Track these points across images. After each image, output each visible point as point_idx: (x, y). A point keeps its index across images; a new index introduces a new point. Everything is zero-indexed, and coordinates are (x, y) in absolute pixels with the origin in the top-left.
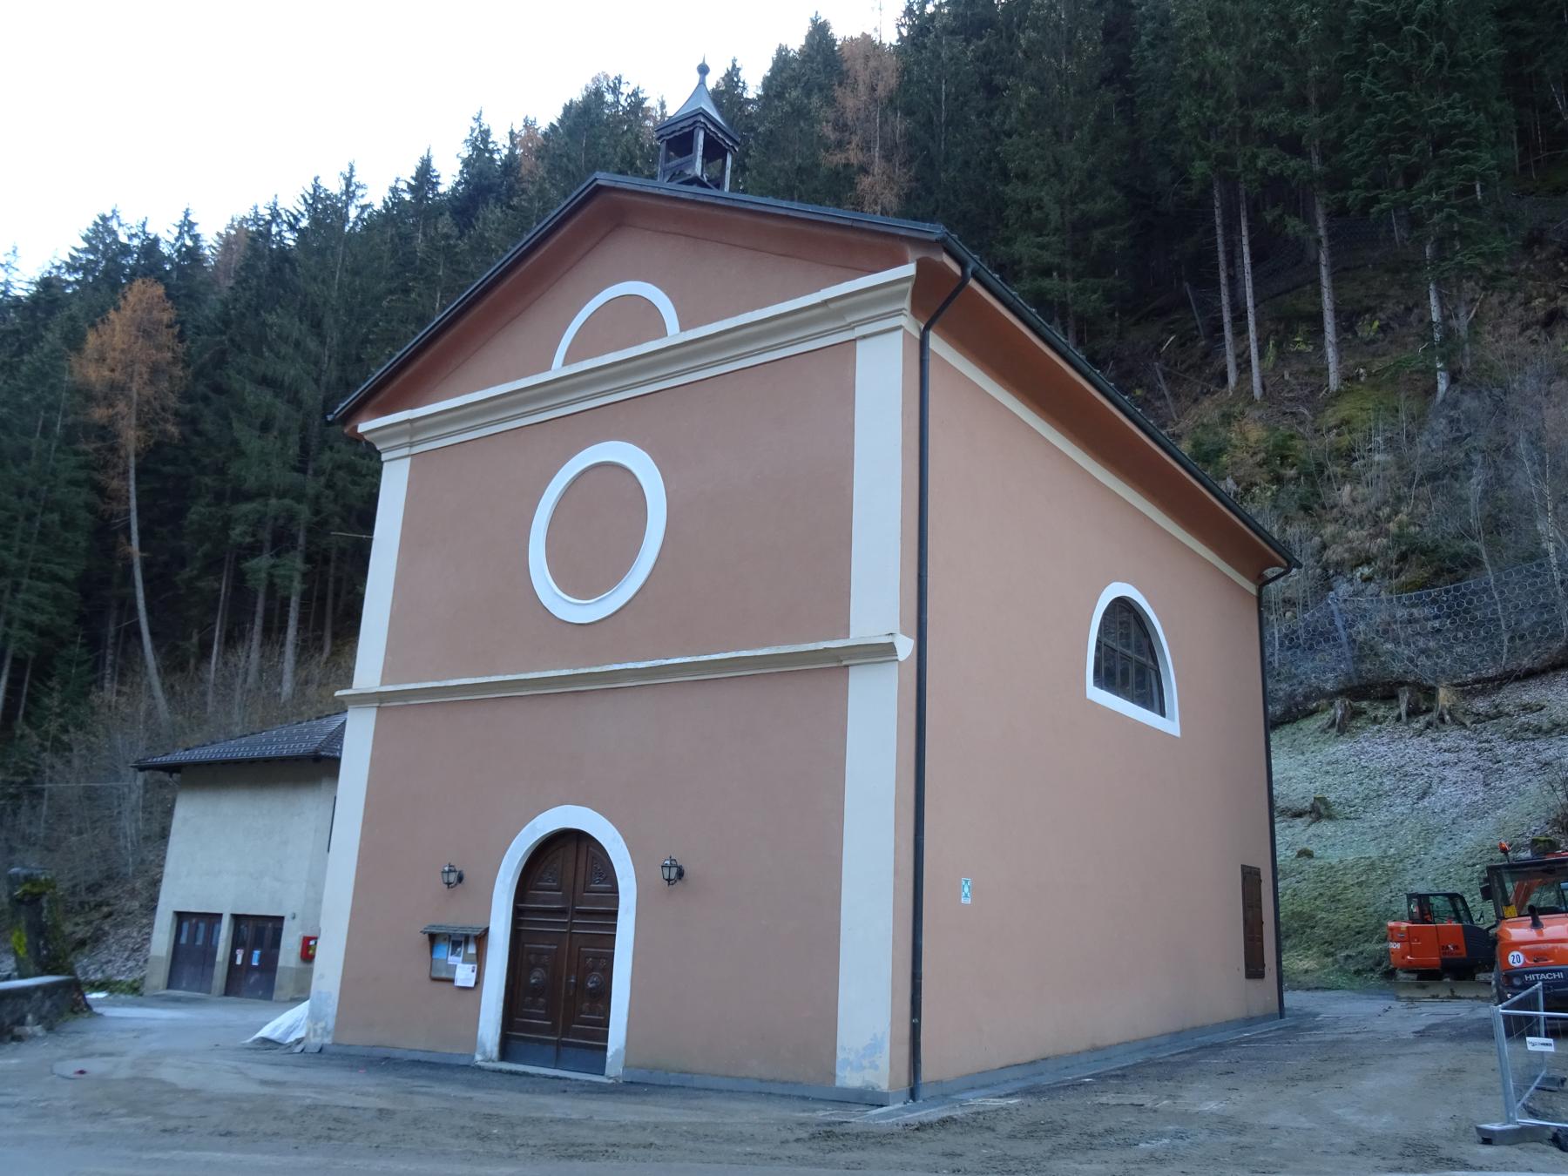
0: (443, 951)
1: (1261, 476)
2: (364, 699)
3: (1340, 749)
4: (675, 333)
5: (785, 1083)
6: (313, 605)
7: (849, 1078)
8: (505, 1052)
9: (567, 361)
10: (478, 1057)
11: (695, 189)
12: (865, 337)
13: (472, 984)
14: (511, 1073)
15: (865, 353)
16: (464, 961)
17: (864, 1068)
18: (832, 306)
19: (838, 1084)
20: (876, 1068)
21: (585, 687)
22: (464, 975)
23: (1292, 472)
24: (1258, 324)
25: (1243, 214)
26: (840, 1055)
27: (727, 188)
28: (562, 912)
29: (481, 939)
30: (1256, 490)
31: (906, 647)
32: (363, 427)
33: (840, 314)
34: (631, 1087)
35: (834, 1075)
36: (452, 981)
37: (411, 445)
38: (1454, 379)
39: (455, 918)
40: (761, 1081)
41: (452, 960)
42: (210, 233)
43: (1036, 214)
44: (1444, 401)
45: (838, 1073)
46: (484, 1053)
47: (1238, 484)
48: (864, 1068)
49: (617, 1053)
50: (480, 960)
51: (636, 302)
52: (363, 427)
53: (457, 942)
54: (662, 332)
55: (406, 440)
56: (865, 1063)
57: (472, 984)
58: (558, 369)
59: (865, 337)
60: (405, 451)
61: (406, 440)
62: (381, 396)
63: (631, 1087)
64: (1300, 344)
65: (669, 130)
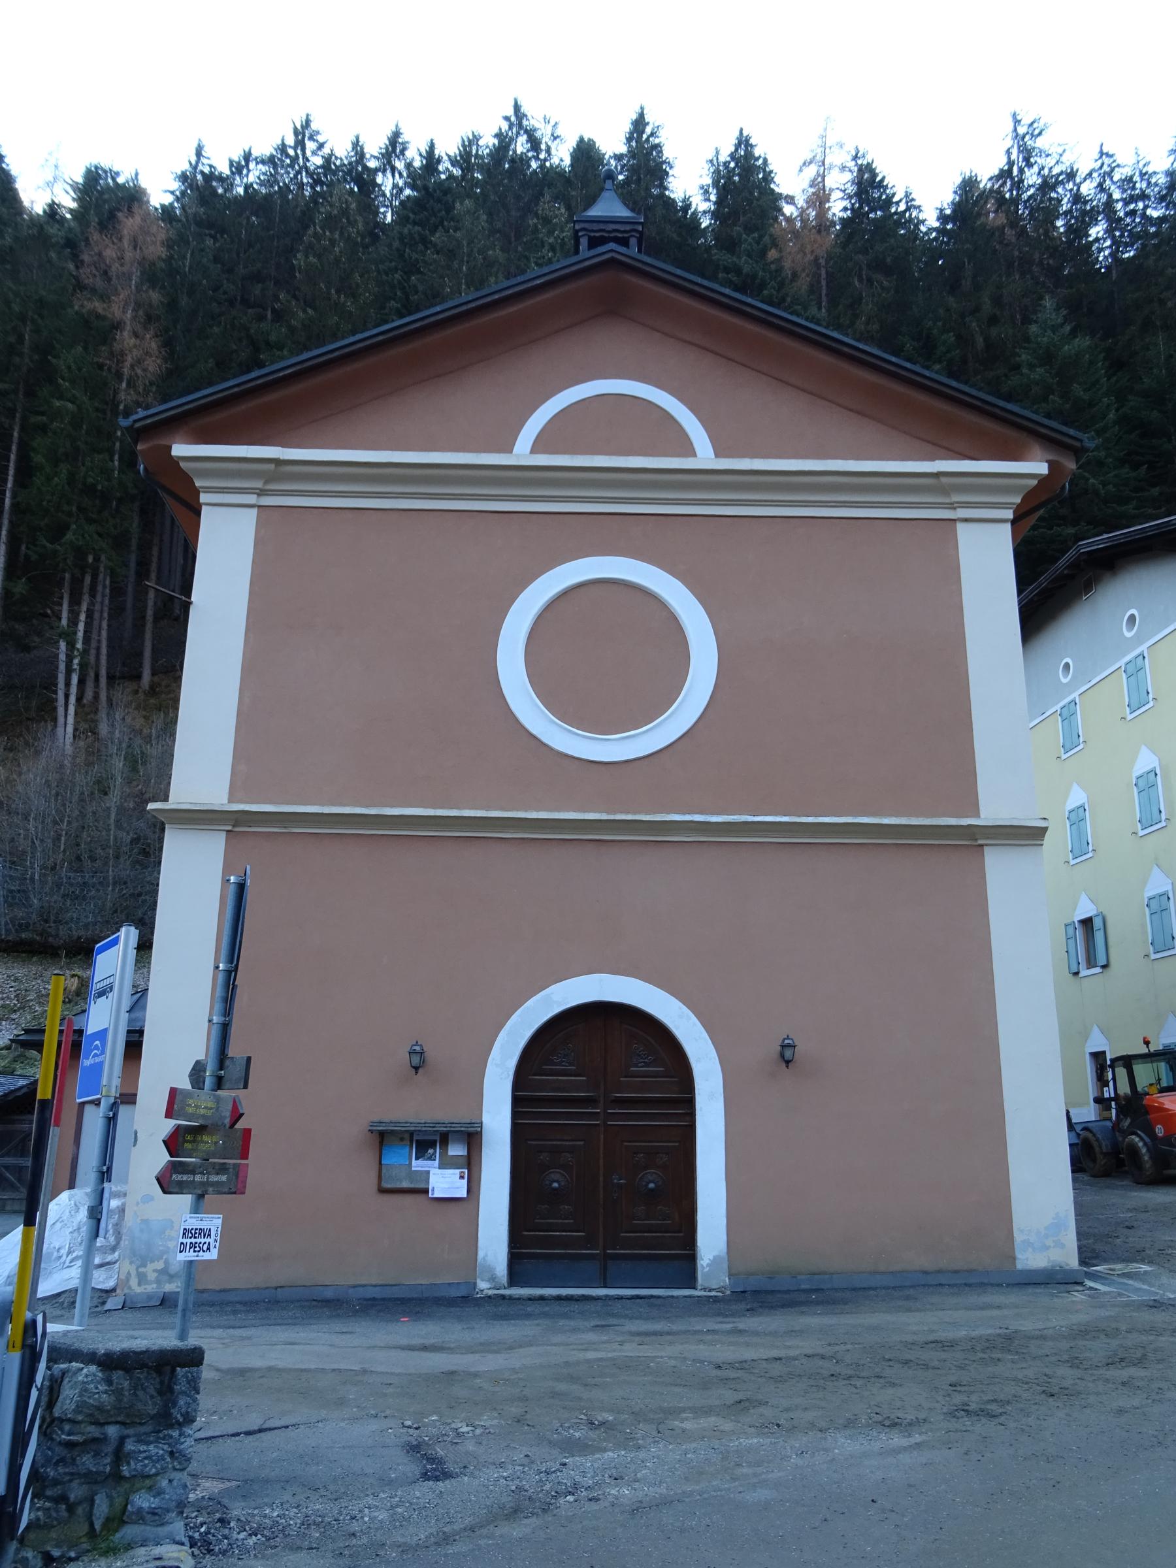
2: (199, 818)
3: (6, 1274)
4: (705, 455)
5: (956, 1272)
6: (124, 670)
7: (1030, 1259)
8: (516, 1275)
9: (539, 446)
10: (483, 1285)
12: (966, 520)
13: (463, 1193)
14: (559, 1298)
15: (965, 534)
17: (1048, 1248)
18: (944, 480)
19: (1019, 1266)
20: (1062, 1246)
21: (610, 837)
22: (445, 1182)
26: (1018, 1237)
29: (473, 1138)
32: (179, 450)
33: (945, 491)
34: (715, 1305)
35: (1014, 1259)
36: (426, 1191)
37: (261, 493)
39: (417, 1108)
40: (925, 1273)
42: (928, 195)
45: (1019, 1255)
46: (492, 1279)
48: (1048, 1248)
49: (716, 1261)
50: (471, 1165)
52: (179, 450)
53: (427, 1141)
55: (259, 484)
56: (1049, 1242)
57: (463, 1193)
58: (522, 451)
59: (966, 520)
60: (252, 499)
61: (259, 484)
62: (218, 417)
63: (715, 1305)
65: (595, 227)
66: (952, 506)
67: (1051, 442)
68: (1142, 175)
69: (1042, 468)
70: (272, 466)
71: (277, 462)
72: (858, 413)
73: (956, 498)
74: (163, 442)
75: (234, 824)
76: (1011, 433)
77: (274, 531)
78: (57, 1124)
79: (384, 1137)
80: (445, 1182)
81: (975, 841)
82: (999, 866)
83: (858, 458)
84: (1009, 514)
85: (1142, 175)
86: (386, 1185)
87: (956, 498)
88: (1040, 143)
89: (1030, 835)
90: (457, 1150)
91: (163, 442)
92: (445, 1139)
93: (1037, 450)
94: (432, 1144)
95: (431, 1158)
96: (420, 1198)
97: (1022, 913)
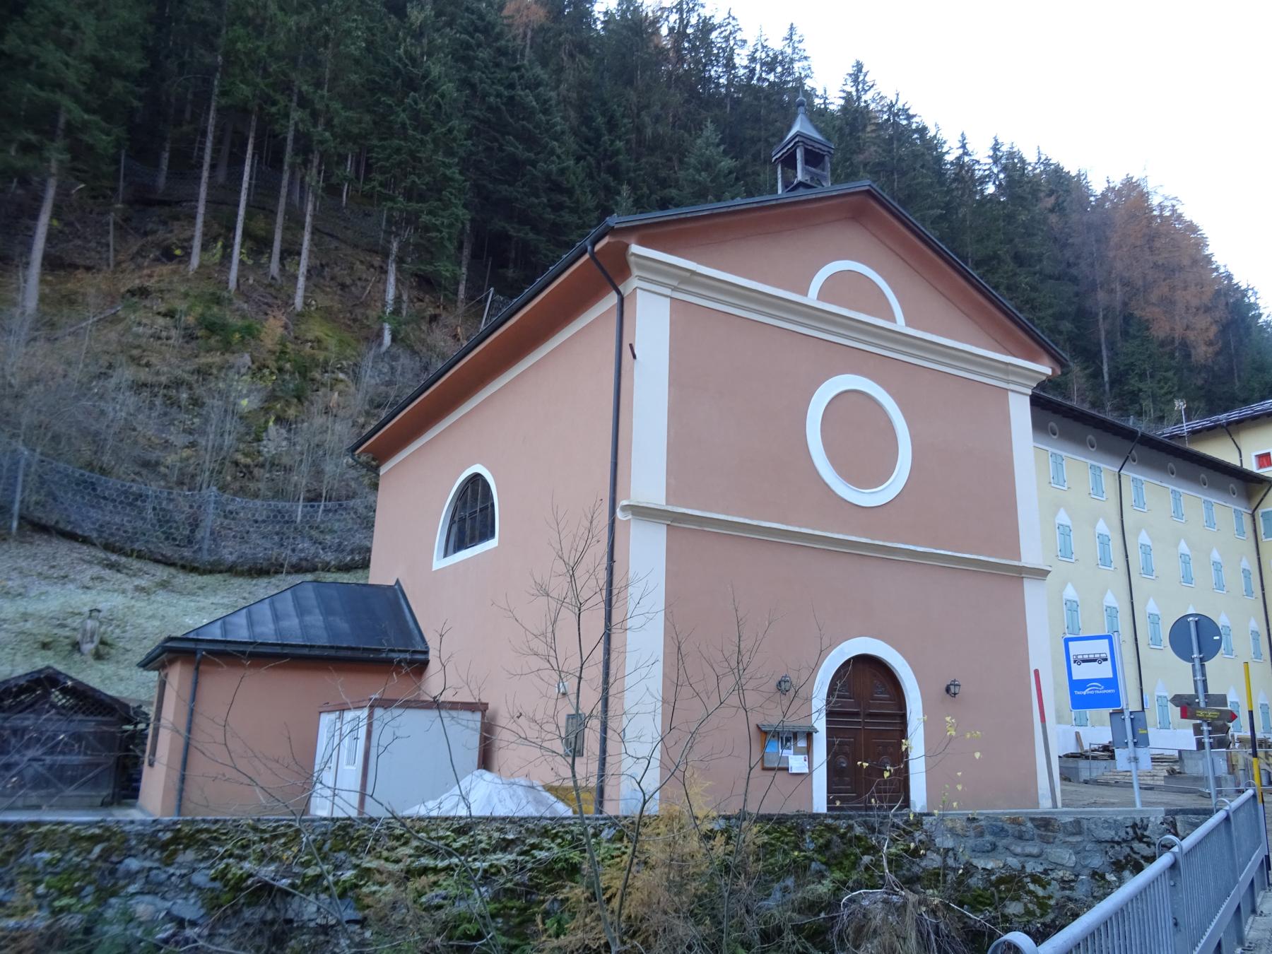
0: (774, 748)
1: (272, 364)
4: (900, 325)
11: (801, 191)
13: (806, 771)
16: (795, 754)
21: (862, 552)
22: (797, 763)
23: (288, 366)
24: (205, 223)
25: (251, 141)
27: (780, 192)
28: (856, 714)
30: (266, 372)
31: (619, 515)
33: (1007, 372)
37: (675, 289)
38: (394, 340)
41: (786, 753)
43: (66, 31)
44: (387, 352)
47: (253, 362)
50: (809, 751)
51: (844, 274)
52: (635, 249)
54: (805, 293)
58: (812, 298)
60: (668, 292)
61: (675, 283)
64: (264, 260)
66: (1008, 382)
67: (1056, 359)
68: (763, 47)
69: (1049, 371)
70: (688, 274)
71: (693, 273)
72: (968, 316)
73: (1011, 378)
74: (625, 240)
75: (672, 521)
76: (1036, 347)
77: (685, 319)
78: (1255, 634)
79: (766, 734)
80: (797, 763)
81: (1021, 573)
82: (1032, 592)
83: (977, 346)
84: (1030, 392)
85: (763, 47)
86: (767, 765)
87: (1011, 378)
88: (800, 46)
89: (1041, 574)
90: (802, 744)
91: (625, 240)
92: (795, 736)
93: (1046, 359)
94: (788, 740)
95: (789, 748)
96: (784, 773)
97: (1040, 613)
